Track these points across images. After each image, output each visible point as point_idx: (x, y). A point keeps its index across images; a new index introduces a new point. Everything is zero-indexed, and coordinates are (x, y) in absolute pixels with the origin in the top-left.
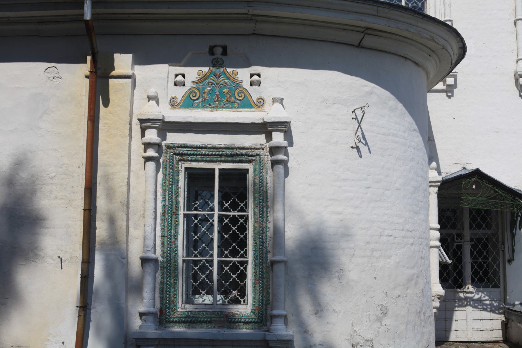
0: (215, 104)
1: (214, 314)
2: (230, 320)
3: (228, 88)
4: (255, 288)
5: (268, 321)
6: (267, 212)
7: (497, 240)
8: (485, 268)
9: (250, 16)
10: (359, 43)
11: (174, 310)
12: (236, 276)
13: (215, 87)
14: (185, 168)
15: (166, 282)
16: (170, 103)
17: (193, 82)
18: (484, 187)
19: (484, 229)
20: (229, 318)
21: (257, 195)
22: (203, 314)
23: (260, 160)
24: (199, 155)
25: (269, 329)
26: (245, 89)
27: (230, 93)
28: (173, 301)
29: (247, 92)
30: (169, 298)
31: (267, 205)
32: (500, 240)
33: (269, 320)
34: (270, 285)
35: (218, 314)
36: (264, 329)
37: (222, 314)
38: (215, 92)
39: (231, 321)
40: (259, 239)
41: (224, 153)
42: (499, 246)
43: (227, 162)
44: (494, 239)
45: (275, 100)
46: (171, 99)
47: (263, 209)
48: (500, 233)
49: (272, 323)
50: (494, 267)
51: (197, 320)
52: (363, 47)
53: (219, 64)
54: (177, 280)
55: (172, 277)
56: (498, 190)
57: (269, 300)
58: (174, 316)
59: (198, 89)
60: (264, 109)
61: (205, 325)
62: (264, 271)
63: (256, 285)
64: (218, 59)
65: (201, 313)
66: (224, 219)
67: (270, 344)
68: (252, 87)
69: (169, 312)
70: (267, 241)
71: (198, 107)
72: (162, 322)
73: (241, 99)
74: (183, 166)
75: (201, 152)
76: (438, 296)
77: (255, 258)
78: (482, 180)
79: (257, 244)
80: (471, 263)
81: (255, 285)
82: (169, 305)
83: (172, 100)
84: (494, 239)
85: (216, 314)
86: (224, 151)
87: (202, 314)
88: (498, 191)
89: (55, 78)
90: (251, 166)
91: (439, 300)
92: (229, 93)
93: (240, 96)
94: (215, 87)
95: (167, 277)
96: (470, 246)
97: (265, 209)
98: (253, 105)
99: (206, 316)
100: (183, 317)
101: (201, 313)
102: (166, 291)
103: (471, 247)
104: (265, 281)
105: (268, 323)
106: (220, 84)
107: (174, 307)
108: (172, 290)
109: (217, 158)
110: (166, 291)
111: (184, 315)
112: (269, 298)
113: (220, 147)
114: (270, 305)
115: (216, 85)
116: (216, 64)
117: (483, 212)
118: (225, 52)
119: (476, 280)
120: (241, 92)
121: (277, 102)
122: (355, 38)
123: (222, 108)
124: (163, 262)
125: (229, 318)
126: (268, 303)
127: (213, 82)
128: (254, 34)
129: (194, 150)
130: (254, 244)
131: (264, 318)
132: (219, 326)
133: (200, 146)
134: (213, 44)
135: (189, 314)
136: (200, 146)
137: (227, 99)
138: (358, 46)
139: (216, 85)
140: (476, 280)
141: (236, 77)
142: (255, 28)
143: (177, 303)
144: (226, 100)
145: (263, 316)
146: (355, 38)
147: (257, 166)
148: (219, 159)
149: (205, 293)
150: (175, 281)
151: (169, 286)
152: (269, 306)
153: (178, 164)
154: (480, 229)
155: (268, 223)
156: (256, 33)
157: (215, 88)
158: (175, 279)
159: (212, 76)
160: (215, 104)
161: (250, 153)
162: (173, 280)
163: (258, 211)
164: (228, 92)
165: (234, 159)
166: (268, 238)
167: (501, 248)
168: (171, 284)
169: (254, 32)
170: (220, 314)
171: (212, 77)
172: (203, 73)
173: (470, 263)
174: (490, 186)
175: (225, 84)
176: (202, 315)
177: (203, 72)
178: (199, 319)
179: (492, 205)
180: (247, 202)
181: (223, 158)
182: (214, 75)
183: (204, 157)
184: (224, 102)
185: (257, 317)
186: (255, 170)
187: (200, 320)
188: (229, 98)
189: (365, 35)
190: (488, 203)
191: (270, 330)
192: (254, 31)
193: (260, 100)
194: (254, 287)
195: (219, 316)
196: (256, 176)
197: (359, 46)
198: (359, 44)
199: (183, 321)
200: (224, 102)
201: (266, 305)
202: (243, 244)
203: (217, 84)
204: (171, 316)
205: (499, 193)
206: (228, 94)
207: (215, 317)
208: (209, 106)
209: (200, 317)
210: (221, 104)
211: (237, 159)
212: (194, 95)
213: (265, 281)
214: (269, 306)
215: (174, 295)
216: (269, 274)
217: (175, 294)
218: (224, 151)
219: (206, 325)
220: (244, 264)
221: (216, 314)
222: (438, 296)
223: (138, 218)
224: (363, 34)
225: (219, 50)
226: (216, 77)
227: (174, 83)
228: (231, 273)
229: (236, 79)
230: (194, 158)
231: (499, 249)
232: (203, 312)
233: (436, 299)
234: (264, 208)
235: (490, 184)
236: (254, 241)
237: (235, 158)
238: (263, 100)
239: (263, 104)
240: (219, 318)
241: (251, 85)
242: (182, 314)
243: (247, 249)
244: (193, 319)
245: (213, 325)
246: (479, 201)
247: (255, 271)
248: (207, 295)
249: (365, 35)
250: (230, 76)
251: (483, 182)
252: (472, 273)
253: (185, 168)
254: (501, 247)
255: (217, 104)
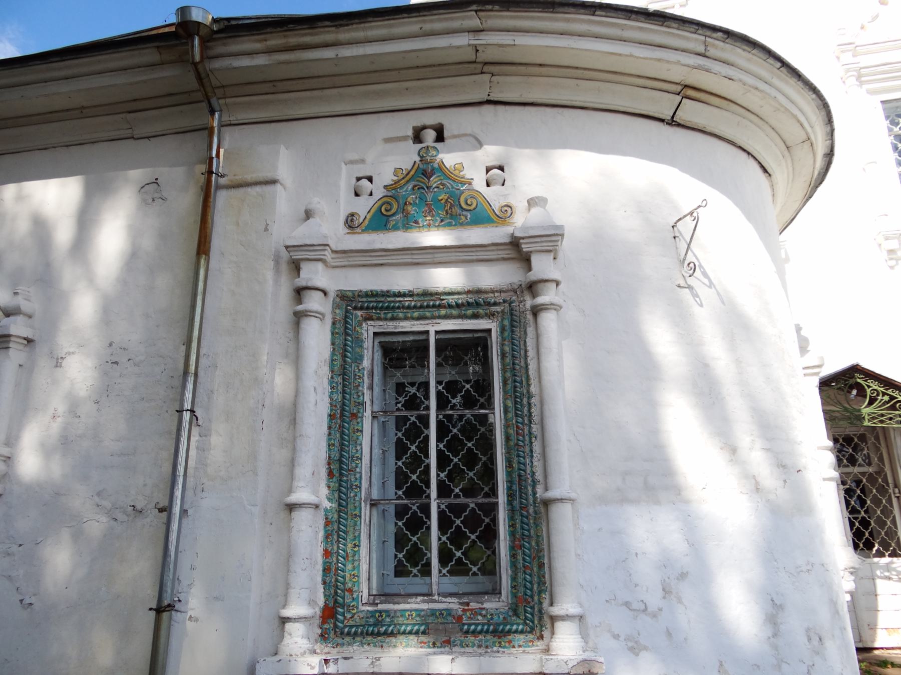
0: (426, 220)
1: (432, 615)
2: (466, 627)
3: (448, 193)
4: (514, 558)
5: (546, 628)
6: (530, 404)
7: (885, 480)
8: (858, 527)
9: (479, 66)
10: (672, 115)
11: (353, 609)
12: (477, 537)
13: (425, 193)
14: (374, 333)
15: (338, 551)
16: (347, 223)
17: (385, 187)
18: (872, 392)
19: (860, 465)
20: (464, 624)
21: (508, 374)
22: (412, 615)
23: (512, 310)
24: (398, 308)
25: (548, 646)
26: (477, 191)
27: (452, 200)
28: (350, 591)
29: (482, 197)
30: (344, 584)
31: (528, 392)
32: (890, 480)
33: (531, 324)
34: (544, 549)
35: (441, 616)
36: (537, 646)
37: (450, 615)
38: (426, 202)
39: (469, 629)
40: (516, 459)
41: (443, 302)
42: (890, 491)
43: (450, 319)
44: (880, 480)
45: (531, 202)
46: (348, 217)
47: (522, 400)
48: (887, 469)
49: (553, 633)
50: (887, 524)
51: (399, 630)
52: (679, 125)
53: (432, 156)
54: (359, 546)
55: (348, 540)
56: (896, 395)
57: (545, 583)
58: (353, 621)
59: (395, 198)
60: (514, 223)
61: (416, 641)
62: (531, 521)
63: (515, 551)
64: (428, 147)
65: (407, 615)
66: (451, 428)
67: (523, 246)
68: (488, 188)
69: (343, 614)
70: (533, 461)
71: (395, 228)
72: (326, 636)
73: (472, 208)
74: (368, 330)
75: (403, 302)
76: (851, 570)
77: (512, 497)
78: (866, 381)
79: (513, 467)
80: (849, 518)
81: (514, 552)
82: (343, 598)
83: (350, 218)
84: (880, 480)
85: (438, 614)
86: (443, 300)
87: (409, 615)
88: (896, 396)
89: (155, 199)
90: (495, 324)
91: (853, 578)
92: (449, 200)
93: (469, 202)
94: (425, 193)
95: (338, 540)
96: (844, 492)
97: (525, 401)
98: (493, 217)
99: (416, 621)
100: (370, 623)
101: (407, 615)
102: (337, 569)
103: (845, 494)
104: (533, 543)
105: (546, 633)
106: (433, 187)
107: (352, 602)
108: (349, 566)
109: (431, 313)
110: (337, 569)
111: (371, 620)
112: (544, 577)
113: (437, 293)
114: (547, 593)
115: (426, 188)
116: (426, 157)
117: (856, 440)
118: (440, 138)
119: (861, 545)
120: (471, 198)
121: (537, 205)
122: (664, 106)
123: (439, 226)
124: (332, 509)
125: (464, 624)
126: (543, 588)
127: (422, 185)
128: (489, 102)
129: (389, 299)
130: (508, 468)
131: (536, 622)
132: (444, 642)
133: (399, 291)
134: (419, 123)
135: (382, 616)
136: (399, 291)
137: (447, 210)
138: (670, 122)
139: (426, 188)
140: (861, 545)
141: (461, 173)
142: (490, 91)
143: (359, 595)
144: (445, 212)
145: (534, 618)
146: (664, 106)
147: (506, 323)
148: (436, 314)
149: (448, 572)
150: (354, 548)
151: (342, 559)
152: (546, 595)
153: (360, 325)
154: (855, 465)
155: (532, 425)
156: (492, 99)
157: (425, 195)
158: (355, 544)
159: (420, 175)
160: (426, 220)
161: (491, 300)
162: (350, 545)
163: (512, 403)
164: (447, 199)
165: (463, 311)
166: (535, 455)
167: (894, 493)
168: (347, 553)
169: (489, 98)
170: (445, 614)
171: (420, 177)
172: (403, 173)
173: (847, 518)
174: (882, 389)
175: (441, 187)
176: (408, 619)
177: (404, 170)
178: (403, 628)
179: (891, 419)
180: (490, 394)
181: (443, 312)
182: (423, 174)
183: (408, 311)
184: (441, 216)
185: (522, 619)
186: (503, 329)
187: (405, 630)
188: (450, 208)
189: (682, 98)
190: (882, 415)
191: (551, 649)
192: (489, 95)
193: (506, 208)
194: (512, 556)
195: (444, 618)
196: (505, 340)
197: (672, 122)
198: (673, 117)
199: (370, 632)
200: (441, 216)
201: (540, 592)
202: (489, 473)
203: (427, 187)
204: (346, 621)
205: (898, 399)
206: (448, 203)
207: (436, 621)
208: (414, 224)
209: (405, 622)
210: (437, 219)
211: (469, 311)
212: (389, 207)
213: (533, 543)
214: (546, 595)
215: (353, 577)
216: (541, 528)
217: (354, 575)
218: (443, 300)
219: (418, 639)
220: (492, 509)
221: (438, 614)
222: (851, 570)
223: (287, 427)
224: (679, 98)
225: (430, 135)
226: (425, 176)
227: (353, 191)
228: (466, 530)
229: (462, 178)
230: (390, 314)
231: (890, 496)
232: (411, 611)
233: (847, 574)
234: (524, 399)
235: (882, 386)
236: (508, 463)
237: (464, 310)
238: (511, 207)
239: (512, 213)
240: (444, 623)
241: (488, 185)
242: (367, 618)
243: (496, 483)
244: (391, 628)
245: (432, 640)
246: (867, 414)
247: (514, 523)
248: (450, 576)
249: (682, 98)
250: (451, 172)
251: (869, 383)
252: (853, 534)
253: (374, 333)
254: (894, 491)
255: (429, 220)
